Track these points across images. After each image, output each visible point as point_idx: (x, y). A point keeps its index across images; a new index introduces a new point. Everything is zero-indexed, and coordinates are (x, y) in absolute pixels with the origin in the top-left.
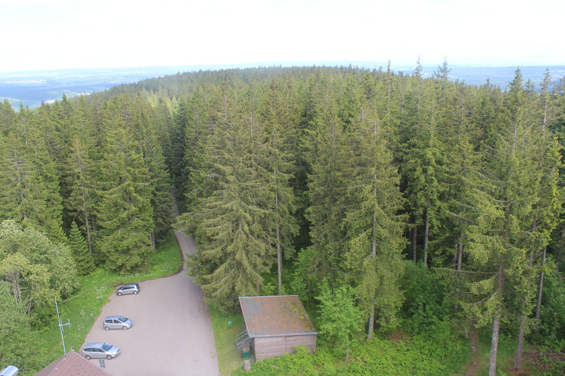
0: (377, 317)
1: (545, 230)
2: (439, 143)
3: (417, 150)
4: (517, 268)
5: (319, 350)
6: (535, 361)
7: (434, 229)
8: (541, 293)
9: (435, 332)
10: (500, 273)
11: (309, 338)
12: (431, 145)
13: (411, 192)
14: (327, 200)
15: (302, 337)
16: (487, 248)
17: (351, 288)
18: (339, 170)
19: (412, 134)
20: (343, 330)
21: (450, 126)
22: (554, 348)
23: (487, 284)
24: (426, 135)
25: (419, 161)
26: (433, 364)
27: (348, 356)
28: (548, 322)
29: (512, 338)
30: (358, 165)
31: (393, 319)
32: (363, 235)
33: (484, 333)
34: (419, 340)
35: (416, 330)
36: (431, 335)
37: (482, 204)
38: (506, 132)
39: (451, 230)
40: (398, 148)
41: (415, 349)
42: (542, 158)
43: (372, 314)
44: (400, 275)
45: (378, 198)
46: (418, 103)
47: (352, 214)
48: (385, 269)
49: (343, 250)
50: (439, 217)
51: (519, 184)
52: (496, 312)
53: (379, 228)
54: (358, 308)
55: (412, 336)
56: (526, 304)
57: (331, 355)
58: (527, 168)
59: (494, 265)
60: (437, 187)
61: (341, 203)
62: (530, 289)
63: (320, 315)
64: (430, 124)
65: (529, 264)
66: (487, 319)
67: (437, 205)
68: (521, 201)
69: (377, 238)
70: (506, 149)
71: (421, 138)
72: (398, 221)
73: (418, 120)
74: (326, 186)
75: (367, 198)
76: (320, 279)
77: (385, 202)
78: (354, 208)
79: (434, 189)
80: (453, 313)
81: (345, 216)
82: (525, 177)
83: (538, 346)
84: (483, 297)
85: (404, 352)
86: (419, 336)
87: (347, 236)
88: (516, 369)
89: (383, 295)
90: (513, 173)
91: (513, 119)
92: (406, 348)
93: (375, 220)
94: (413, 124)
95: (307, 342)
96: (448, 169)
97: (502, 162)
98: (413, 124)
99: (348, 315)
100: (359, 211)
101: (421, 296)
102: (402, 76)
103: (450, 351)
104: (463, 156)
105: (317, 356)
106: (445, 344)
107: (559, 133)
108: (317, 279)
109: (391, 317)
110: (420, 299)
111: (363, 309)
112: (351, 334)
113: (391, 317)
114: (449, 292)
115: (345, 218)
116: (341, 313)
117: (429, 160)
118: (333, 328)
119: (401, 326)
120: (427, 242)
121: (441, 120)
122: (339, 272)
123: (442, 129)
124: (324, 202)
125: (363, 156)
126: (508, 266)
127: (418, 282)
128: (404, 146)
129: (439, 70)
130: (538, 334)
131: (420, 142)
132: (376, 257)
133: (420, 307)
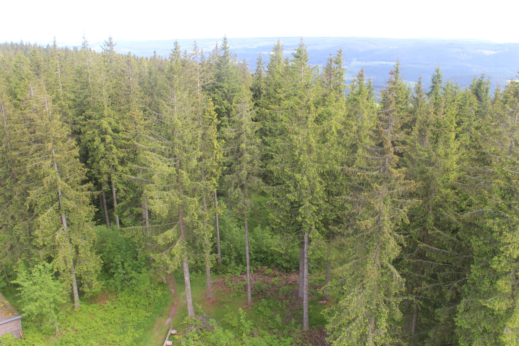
0: (80, 285)
1: (212, 178)
2: (113, 113)
3: (93, 121)
4: (193, 215)
5: (26, 333)
6: (222, 287)
7: (120, 192)
8: (218, 231)
9: (136, 285)
10: (180, 221)
11: (13, 324)
12: (106, 116)
13: (93, 162)
14: (7, 182)
15: (5, 325)
16: (166, 202)
17: (47, 264)
18: (16, 149)
19: (87, 106)
20: (47, 306)
21: (121, 96)
22: (235, 273)
23: (170, 233)
24: (100, 106)
25: (96, 131)
26: (140, 314)
27: (57, 330)
28: (227, 253)
29: (202, 273)
30: (35, 142)
31: (95, 283)
32: (51, 210)
33: (179, 276)
34: (123, 296)
35: (119, 288)
36: (134, 288)
37: (154, 164)
38: (167, 97)
39: (135, 191)
40: (74, 121)
41: (121, 305)
42: (200, 117)
43: (75, 284)
44: (94, 241)
45: (59, 172)
46: (88, 77)
47: (35, 191)
48: (78, 238)
49: (33, 228)
50: (121, 181)
51: (184, 142)
52: (183, 256)
53: (65, 201)
54: (58, 282)
55: (117, 294)
56: (205, 243)
57: (40, 334)
58: (188, 127)
59: (175, 215)
60: (117, 153)
61: (22, 182)
62: (206, 230)
63: (20, 298)
64: (102, 95)
65: (203, 209)
66: (176, 264)
67: (120, 170)
68: (187, 157)
69: (65, 210)
70: (168, 113)
71: (95, 109)
72: (82, 190)
73: (90, 93)
74: (4, 167)
75: (48, 173)
76: (15, 261)
77: (68, 175)
78: (36, 185)
79: (115, 156)
80: (149, 264)
81: (28, 195)
82: (188, 136)
83: (223, 275)
84: (170, 245)
85: (112, 311)
86: (123, 292)
87: (35, 214)
88: (210, 299)
89: (81, 263)
90: (177, 133)
91: (172, 86)
92: (113, 307)
93: (60, 193)
94: (86, 97)
95: (12, 329)
96: (124, 136)
97: (167, 125)
98: (86, 97)
99: (50, 291)
100: (42, 188)
101: (118, 256)
102: (77, 51)
103: (152, 299)
104: (135, 122)
105: (25, 339)
106: (148, 293)
107: (214, 95)
108: (12, 262)
109: (94, 282)
110: (118, 259)
111: (64, 281)
112: (57, 308)
113: (94, 282)
114: (140, 247)
115: (29, 196)
116: (42, 290)
117: (106, 129)
118: (36, 307)
119: (105, 287)
120: (116, 205)
121: (112, 91)
122: (33, 251)
123: (114, 101)
124: (5, 184)
125: (38, 133)
126: (185, 214)
127: (113, 244)
128: (80, 118)
129: (106, 44)
130: (222, 265)
131: (95, 113)
132: (67, 229)
133: (119, 266)
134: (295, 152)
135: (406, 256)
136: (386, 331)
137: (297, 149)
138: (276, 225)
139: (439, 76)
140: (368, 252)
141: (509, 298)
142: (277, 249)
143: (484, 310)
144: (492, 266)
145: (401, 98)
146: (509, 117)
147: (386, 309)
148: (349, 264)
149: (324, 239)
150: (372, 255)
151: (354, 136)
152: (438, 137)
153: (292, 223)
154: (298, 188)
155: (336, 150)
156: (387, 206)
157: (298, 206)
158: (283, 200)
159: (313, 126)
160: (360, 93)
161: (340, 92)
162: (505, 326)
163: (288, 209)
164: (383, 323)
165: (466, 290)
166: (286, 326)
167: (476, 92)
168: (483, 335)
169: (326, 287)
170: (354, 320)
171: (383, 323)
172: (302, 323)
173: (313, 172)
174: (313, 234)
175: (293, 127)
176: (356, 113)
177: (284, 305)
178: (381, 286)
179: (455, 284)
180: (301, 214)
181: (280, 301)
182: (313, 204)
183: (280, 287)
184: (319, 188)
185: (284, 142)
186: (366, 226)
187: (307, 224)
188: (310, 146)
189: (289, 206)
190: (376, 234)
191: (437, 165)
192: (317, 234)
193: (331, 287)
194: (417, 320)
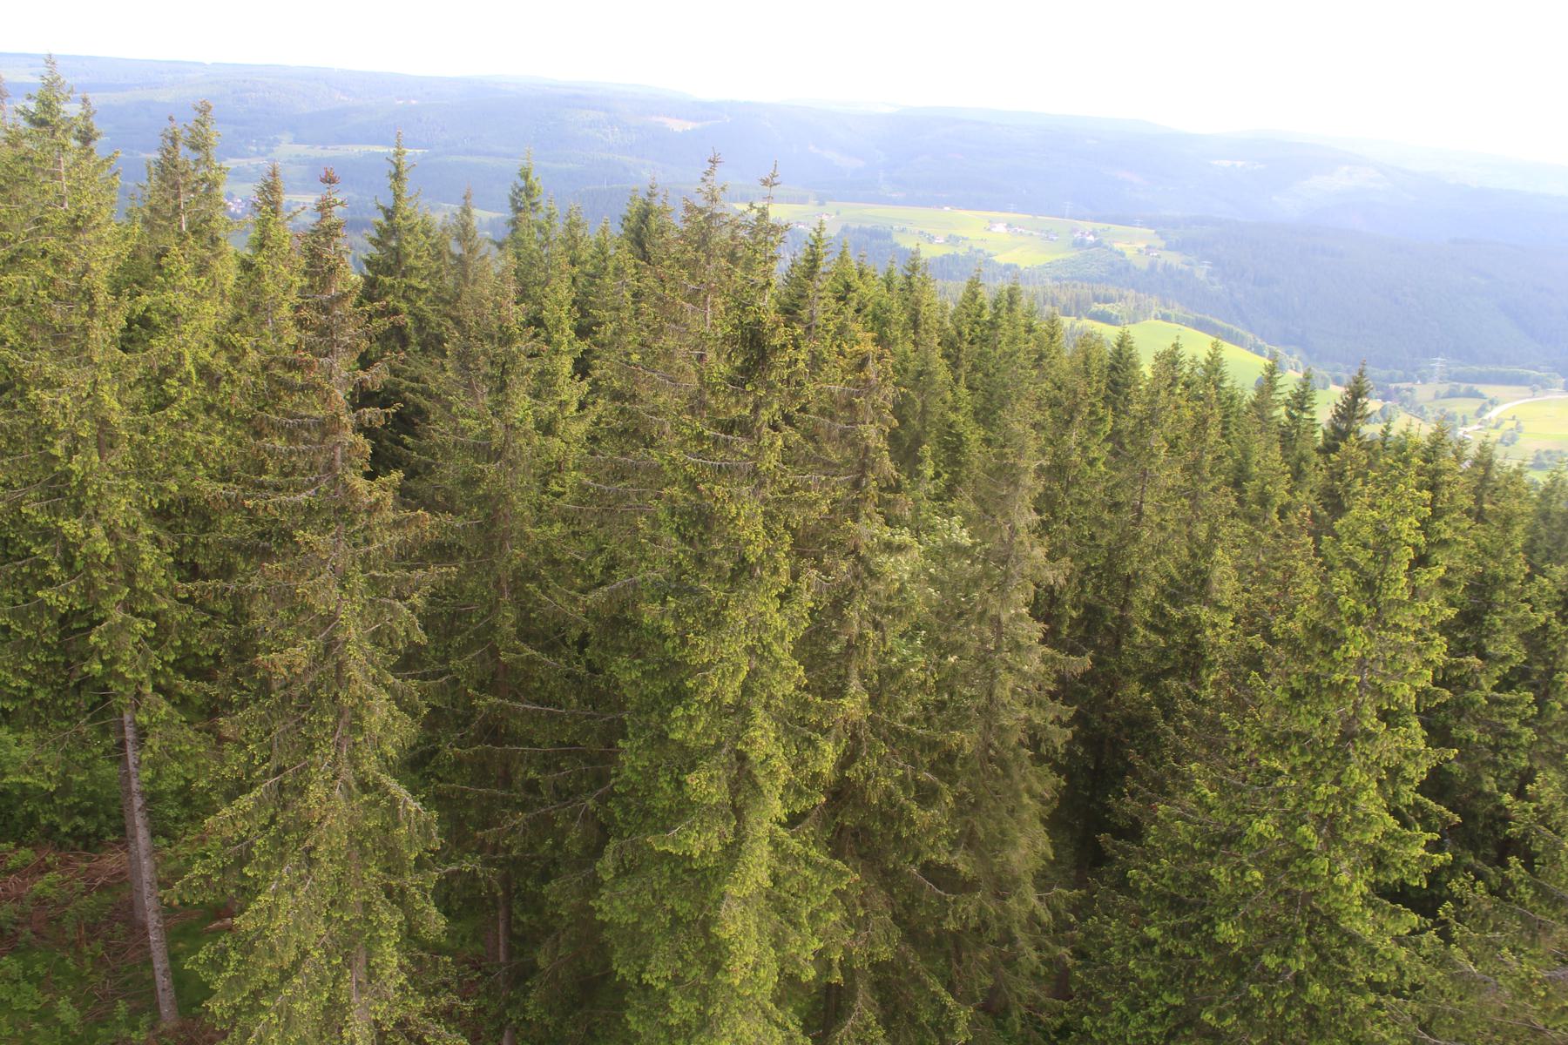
134: (52, 445)
135: (449, 740)
136: (402, 978)
137: (58, 435)
138: (13, 698)
139: (532, 189)
140: (310, 747)
141: (726, 818)
142: (28, 780)
143: (669, 864)
144: (671, 736)
145: (417, 257)
146: (688, 306)
147: (393, 913)
148: (252, 795)
149: (190, 723)
150: (325, 753)
151: (254, 384)
152: (504, 372)
153: (71, 684)
154: (79, 565)
155: (206, 430)
156: (352, 596)
157: (85, 624)
158: (29, 612)
159: (108, 356)
160: (262, 246)
161: (214, 241)
162: (723, 896)
163: (52, 639)
164: (388, 958)
165: (618, 814)
166: (100, 1031)
167: (638, 236)
168: (673, 933)
169: (190, 881)
170: (296, 965)
171: (391, 958)
172: (155, 1008)
173: (121, 508)
174: (148, 712)
175: (37, 363)
176: (254, 309)
177: (87, 961)
178: (368, 845)
179: (590, 803)
180: (101, 653)
181: (72, 950)
182: (138, 615)
183: (67, 904)
184: (149, 558)
185: (11, 416)
186: (289, 668)
187: (126, 682)
188: (105, 422)
189: (53, 630)
190: (329, 689)
191: (510, 456)
192: (164, 708)
193: (207, 878)
194: (508, 925)
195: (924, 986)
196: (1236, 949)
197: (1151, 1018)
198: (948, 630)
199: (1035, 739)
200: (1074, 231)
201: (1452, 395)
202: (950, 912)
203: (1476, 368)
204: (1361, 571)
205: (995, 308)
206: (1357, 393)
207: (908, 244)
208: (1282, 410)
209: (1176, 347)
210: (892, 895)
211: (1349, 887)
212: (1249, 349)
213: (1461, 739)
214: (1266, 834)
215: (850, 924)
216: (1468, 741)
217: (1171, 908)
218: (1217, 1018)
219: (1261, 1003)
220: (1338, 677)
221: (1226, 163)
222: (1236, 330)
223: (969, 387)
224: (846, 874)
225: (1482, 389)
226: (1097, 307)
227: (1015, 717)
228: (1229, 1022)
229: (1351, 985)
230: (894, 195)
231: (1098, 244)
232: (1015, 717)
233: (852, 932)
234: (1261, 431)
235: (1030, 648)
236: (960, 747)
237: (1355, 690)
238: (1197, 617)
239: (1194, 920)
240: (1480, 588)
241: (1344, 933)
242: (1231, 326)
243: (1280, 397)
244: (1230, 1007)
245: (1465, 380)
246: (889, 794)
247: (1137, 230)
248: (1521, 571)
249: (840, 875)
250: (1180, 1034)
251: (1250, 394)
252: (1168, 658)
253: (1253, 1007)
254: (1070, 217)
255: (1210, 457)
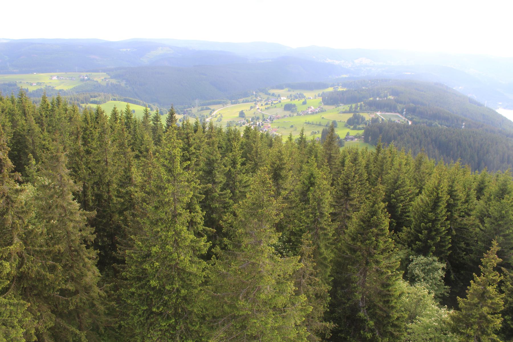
195: (68, 330)
196: (158, 287)
197: (140, 316)
198: (47, 213)
199: (85, 241)
200: (80, 76)
201: (202, 110)
202: (70, 304)
203: (207, 101)
204: (167, 167)
205: (52, 104)
206: (172, 114)
207: (25, 87)
208: (151, 122)
209: (115, 108)
210: (49, 304)
211: (184, 259)
212: (142, 105)
213: (214, 208)
214: (157, 251)
215: (36, 319)
216: (216, 207)
217: (138, 280)
218: (157, 309)
219: (169, 300)
220: (167, 200)
221: (125, 50)
222: (137, 100)
223: (49, 132)
224: (25, 304)
225: (210, 107)
226: (92, 99)
227: (76, 236)
228: (161, 309)
229: (193, 287)
230: (15, 71)
231: (89, 79)
232: (76, 236)
233: (37, 321)
234: (146, 130)
235: (75, 213)
236: (59, 251)
237: (172, 202)
238: (130, 190)
239: (144, 283)
240: (210, 164)
241: (188, 273)
242: (135, 99)
243: (150, 119)
244: (160, 305)
245: (205, 105)
246: (38, 272)
247: (101, 73)
248: (219, 157)
249: (23, 305)
250: (150, 317)
251: (141, 119)
252: (125, 205)
253: (167, 302)
254: (78, 72)
255: (127, 141)
